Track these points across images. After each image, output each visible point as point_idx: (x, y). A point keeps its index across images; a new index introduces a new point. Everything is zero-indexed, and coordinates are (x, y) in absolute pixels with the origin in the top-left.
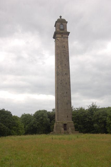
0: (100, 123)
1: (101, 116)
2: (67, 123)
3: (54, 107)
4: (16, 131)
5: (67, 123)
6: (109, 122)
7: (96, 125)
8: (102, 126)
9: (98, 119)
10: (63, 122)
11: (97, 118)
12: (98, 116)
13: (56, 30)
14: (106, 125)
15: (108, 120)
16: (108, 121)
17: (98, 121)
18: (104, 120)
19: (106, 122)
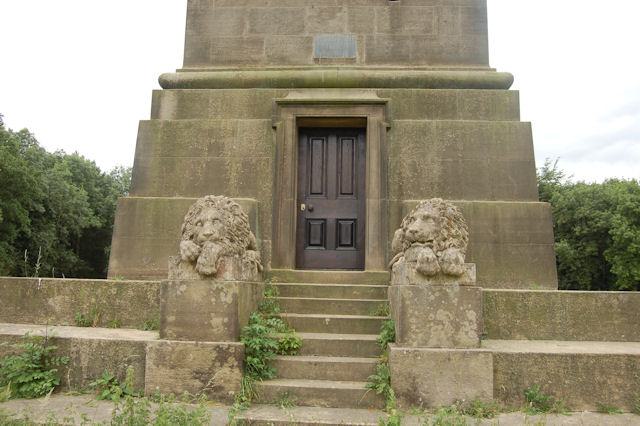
0: (578, 239)
1: (584, 211)
2: (370, 95)
3: (128, 162)
4: (137, 412)
5: (370, 95)
6: (623, 233)
7: (566, 245)
8: (589, 249)
9: (573, 223)
10: (300, 84)
11: (568, 217)
12: (571, 208)
13: (197, 50)
14: (607, 247)
15: (620, 225)
16: (621, 228)
17: (570, 231)
18: (599, 225)
19: (611, 236)
